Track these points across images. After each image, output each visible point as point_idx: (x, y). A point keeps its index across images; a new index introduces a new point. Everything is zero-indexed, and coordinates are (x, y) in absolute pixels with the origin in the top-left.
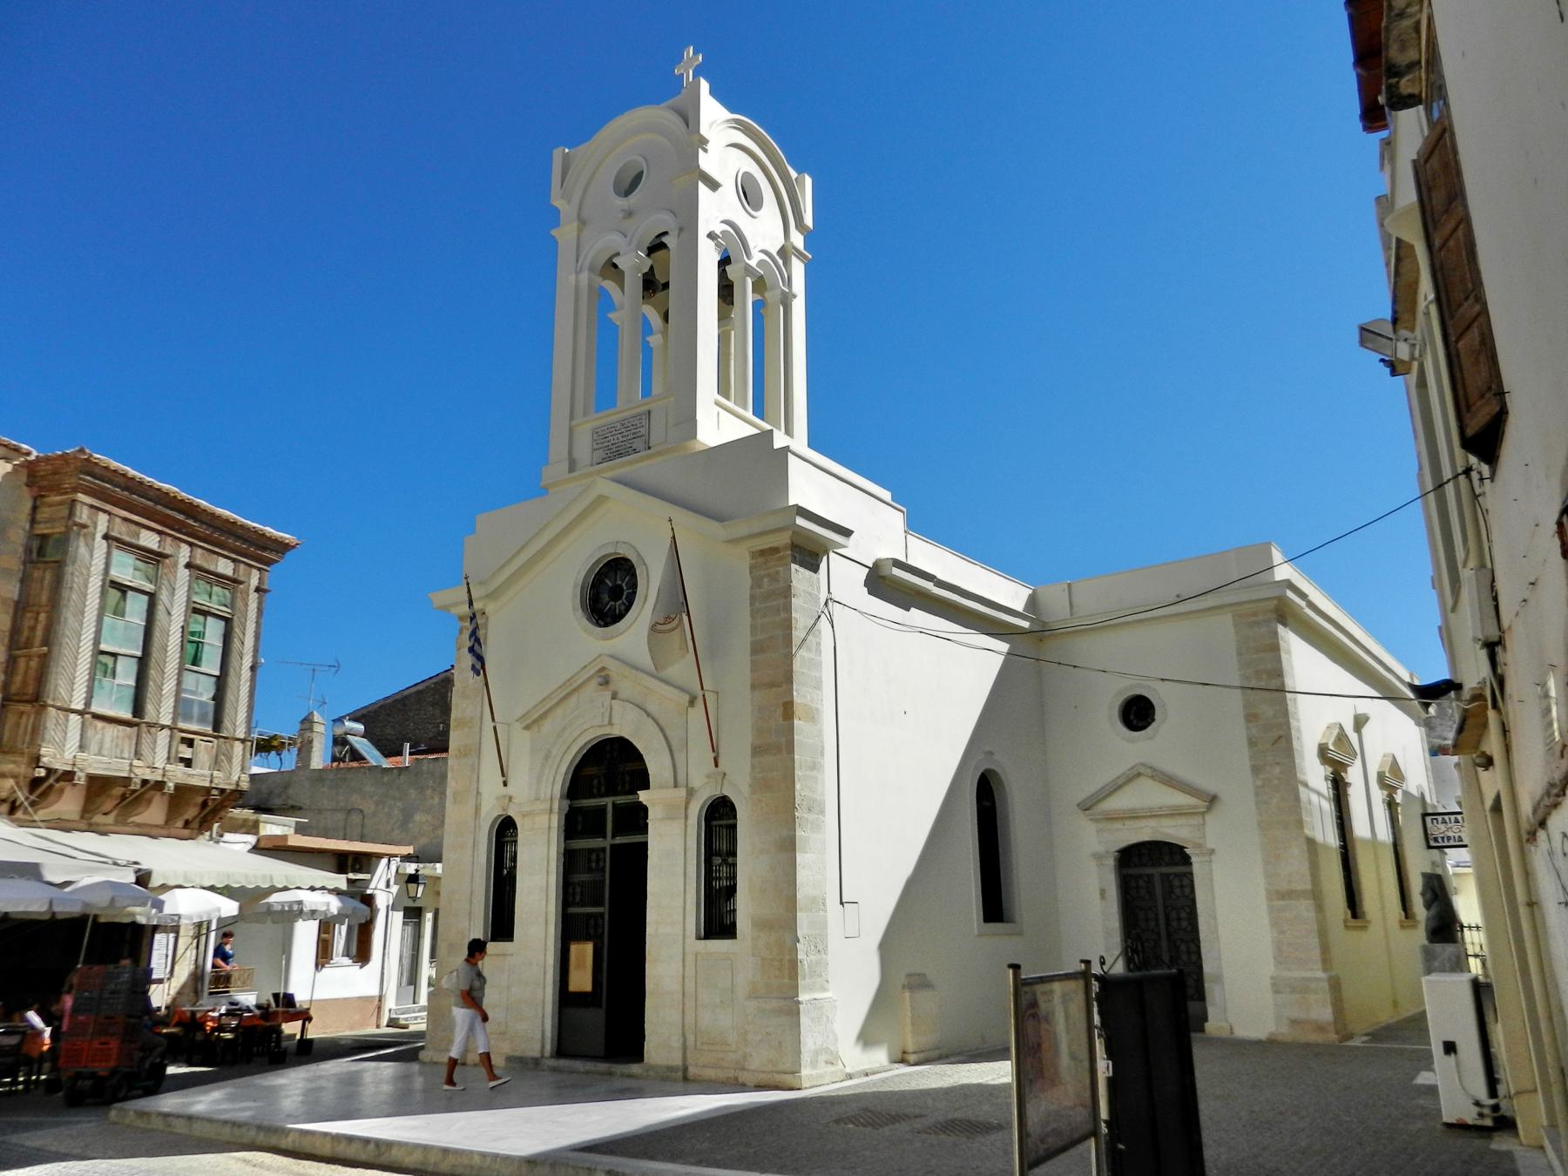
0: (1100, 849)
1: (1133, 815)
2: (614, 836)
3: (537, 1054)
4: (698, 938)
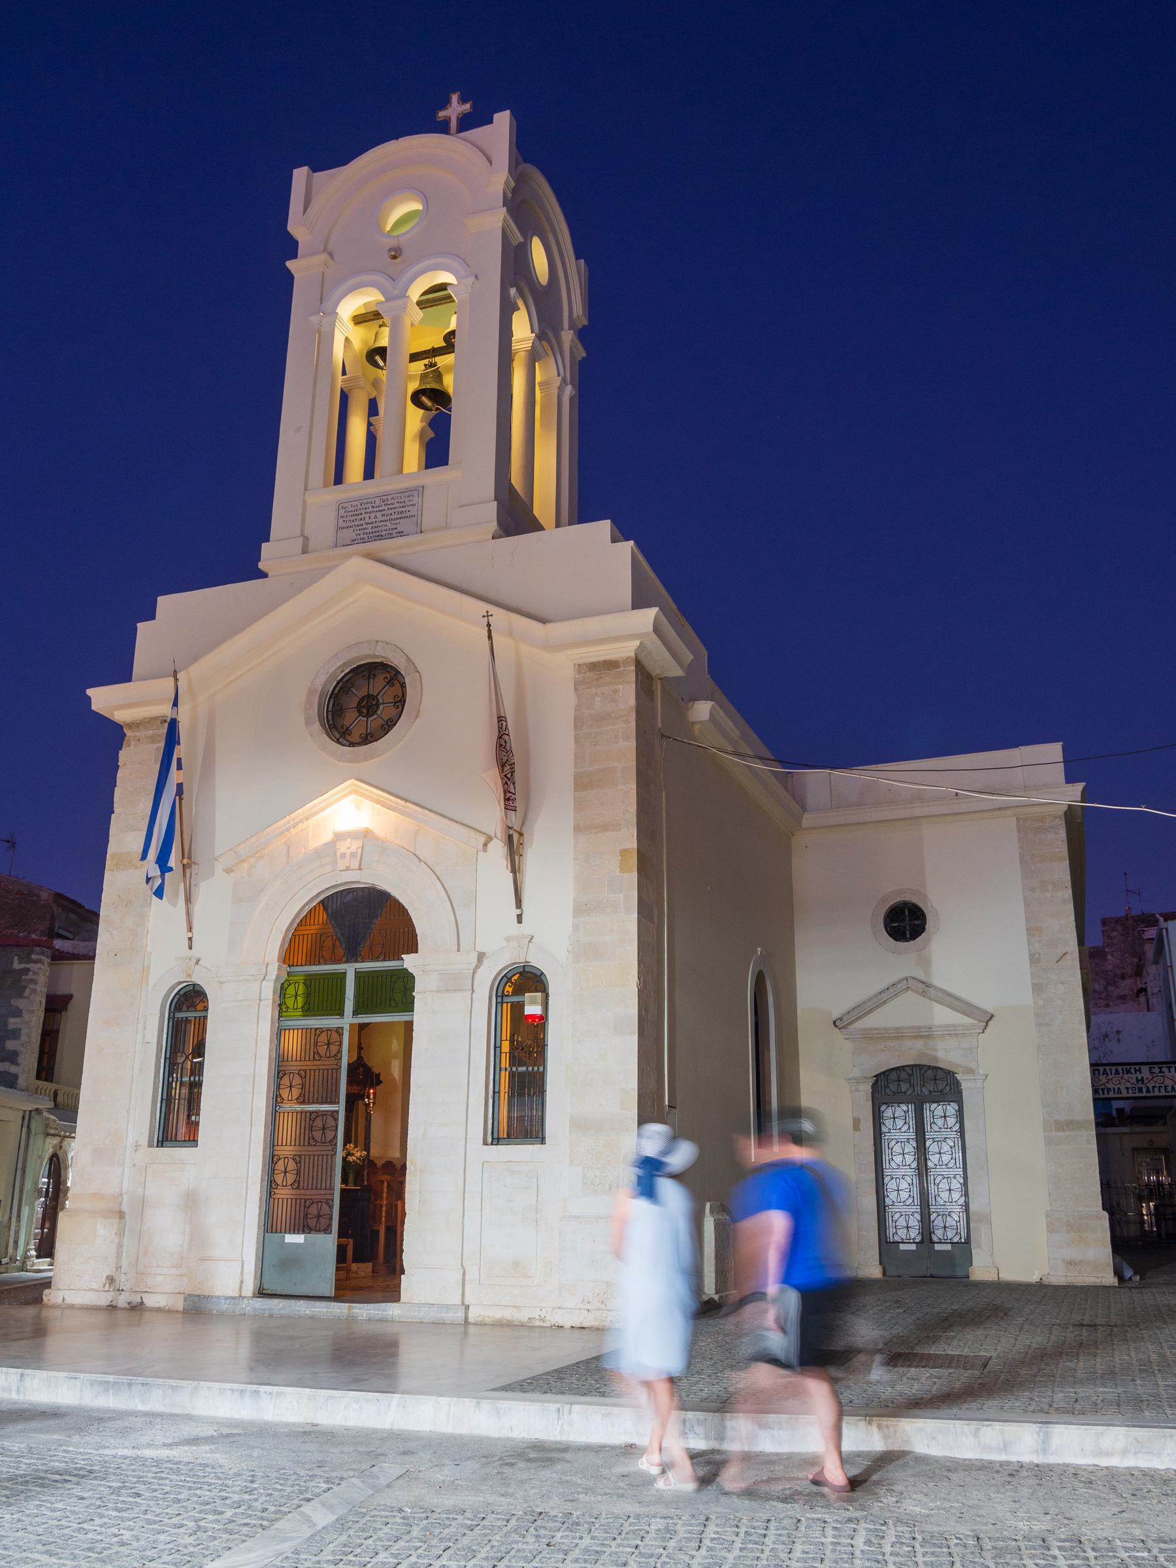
0: (857, 1073)
1: (898, 1035)
2: (356, 1013)
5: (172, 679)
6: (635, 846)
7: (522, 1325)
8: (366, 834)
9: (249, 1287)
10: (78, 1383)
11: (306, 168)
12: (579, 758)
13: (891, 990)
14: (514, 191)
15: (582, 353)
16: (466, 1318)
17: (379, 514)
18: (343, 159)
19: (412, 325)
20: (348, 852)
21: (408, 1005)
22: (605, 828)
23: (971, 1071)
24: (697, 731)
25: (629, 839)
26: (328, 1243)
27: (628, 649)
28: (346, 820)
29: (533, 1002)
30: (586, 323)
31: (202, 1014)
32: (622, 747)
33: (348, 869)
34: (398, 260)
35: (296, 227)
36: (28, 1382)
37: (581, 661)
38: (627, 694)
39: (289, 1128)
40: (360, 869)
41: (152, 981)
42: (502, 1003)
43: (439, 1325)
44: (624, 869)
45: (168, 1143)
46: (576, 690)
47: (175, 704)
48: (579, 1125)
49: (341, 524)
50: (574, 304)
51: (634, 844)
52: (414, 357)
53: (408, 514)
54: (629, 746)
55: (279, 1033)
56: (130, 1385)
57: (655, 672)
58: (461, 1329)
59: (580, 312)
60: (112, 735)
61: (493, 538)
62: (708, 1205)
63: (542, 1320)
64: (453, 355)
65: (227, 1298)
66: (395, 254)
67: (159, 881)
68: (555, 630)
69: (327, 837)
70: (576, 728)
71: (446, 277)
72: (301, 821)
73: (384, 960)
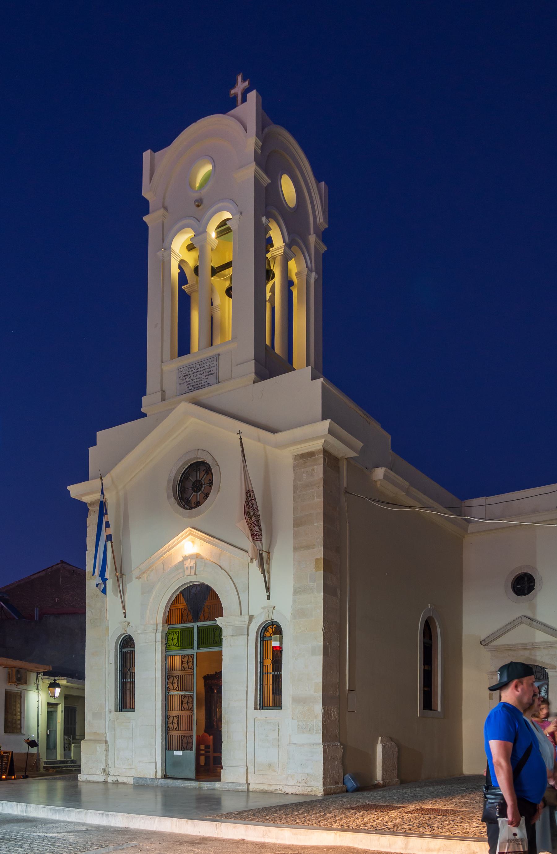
0: (493, 669)
1: (515, 648)
3: (153, 776)
4: (256, 709)
5: (99, 479)
6: (322, 557)
7: (272, 793)
8: (197, 557)
9: (159, 775)
10: (46, 809)
11: (149, 151)
12: (295, 509)
13: (512, 624)
14: (262, 148)
15: (323, 248)
16: (248, 789)
17: (198, 374)
18: (167, 142)
19: (212, 250)
20: (189, 566)
21: (219, 643)
22: (308, 547)
23: (554, 667)
24: (378, 486)
25: (319, 552)
26: (192, 754)
27: (317, 445)
28: (188, 548)
29: (276, 640)
30: (327, 226)
31: (132, 649)
32: (317, 501)
33: (190, 575)
34: (201, 207)
35: (146, 194)
36: (29, 809)
37: (295, 454)
38: (318, 470)
39: (175, 702)
40: (195, 574)
41: (110, 633)
42: (263, 641)
43: (236, 791)
44: (316, 569)
45: (124, 710)
46: (294, 470)
47: (102, 493)
48: (296, 700)
49: (180, 382)
50: (317, 215)
51: (321, 555)
52: (215, 271)
53: (212, 372)
54: (319, 501)
55: (166, 658)
56: (63, 811)
57: (340, 456)
58: (245, 794)
59: (322, 220)
60: (82, 508)
61: (254, 383)
62: (380, 738)
63: (281, 790)
64: (231, 268)
65: (150, 779)
66: (199, 203)
67: (103, 586)
68: (279, 436)
69: (181, 559)
70: (294, 492)
71: (227, 215)
72: (168, 551)
73: (210, 621)
